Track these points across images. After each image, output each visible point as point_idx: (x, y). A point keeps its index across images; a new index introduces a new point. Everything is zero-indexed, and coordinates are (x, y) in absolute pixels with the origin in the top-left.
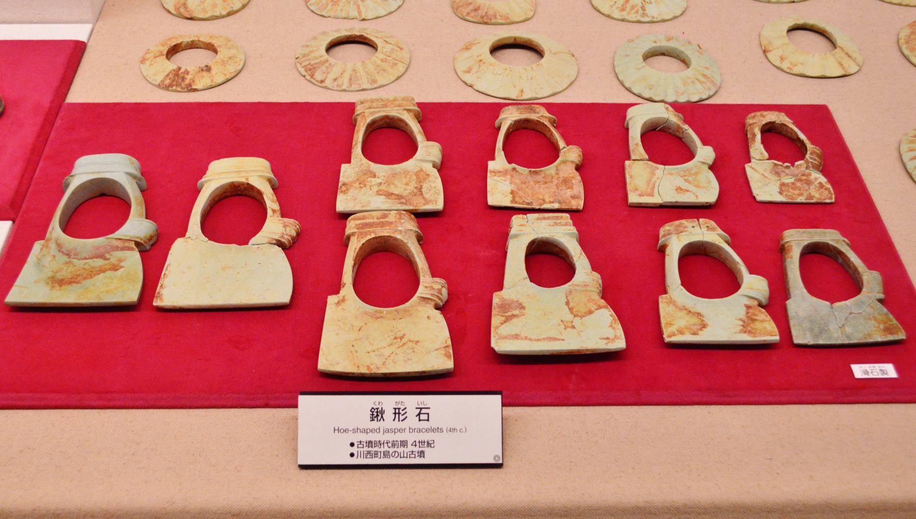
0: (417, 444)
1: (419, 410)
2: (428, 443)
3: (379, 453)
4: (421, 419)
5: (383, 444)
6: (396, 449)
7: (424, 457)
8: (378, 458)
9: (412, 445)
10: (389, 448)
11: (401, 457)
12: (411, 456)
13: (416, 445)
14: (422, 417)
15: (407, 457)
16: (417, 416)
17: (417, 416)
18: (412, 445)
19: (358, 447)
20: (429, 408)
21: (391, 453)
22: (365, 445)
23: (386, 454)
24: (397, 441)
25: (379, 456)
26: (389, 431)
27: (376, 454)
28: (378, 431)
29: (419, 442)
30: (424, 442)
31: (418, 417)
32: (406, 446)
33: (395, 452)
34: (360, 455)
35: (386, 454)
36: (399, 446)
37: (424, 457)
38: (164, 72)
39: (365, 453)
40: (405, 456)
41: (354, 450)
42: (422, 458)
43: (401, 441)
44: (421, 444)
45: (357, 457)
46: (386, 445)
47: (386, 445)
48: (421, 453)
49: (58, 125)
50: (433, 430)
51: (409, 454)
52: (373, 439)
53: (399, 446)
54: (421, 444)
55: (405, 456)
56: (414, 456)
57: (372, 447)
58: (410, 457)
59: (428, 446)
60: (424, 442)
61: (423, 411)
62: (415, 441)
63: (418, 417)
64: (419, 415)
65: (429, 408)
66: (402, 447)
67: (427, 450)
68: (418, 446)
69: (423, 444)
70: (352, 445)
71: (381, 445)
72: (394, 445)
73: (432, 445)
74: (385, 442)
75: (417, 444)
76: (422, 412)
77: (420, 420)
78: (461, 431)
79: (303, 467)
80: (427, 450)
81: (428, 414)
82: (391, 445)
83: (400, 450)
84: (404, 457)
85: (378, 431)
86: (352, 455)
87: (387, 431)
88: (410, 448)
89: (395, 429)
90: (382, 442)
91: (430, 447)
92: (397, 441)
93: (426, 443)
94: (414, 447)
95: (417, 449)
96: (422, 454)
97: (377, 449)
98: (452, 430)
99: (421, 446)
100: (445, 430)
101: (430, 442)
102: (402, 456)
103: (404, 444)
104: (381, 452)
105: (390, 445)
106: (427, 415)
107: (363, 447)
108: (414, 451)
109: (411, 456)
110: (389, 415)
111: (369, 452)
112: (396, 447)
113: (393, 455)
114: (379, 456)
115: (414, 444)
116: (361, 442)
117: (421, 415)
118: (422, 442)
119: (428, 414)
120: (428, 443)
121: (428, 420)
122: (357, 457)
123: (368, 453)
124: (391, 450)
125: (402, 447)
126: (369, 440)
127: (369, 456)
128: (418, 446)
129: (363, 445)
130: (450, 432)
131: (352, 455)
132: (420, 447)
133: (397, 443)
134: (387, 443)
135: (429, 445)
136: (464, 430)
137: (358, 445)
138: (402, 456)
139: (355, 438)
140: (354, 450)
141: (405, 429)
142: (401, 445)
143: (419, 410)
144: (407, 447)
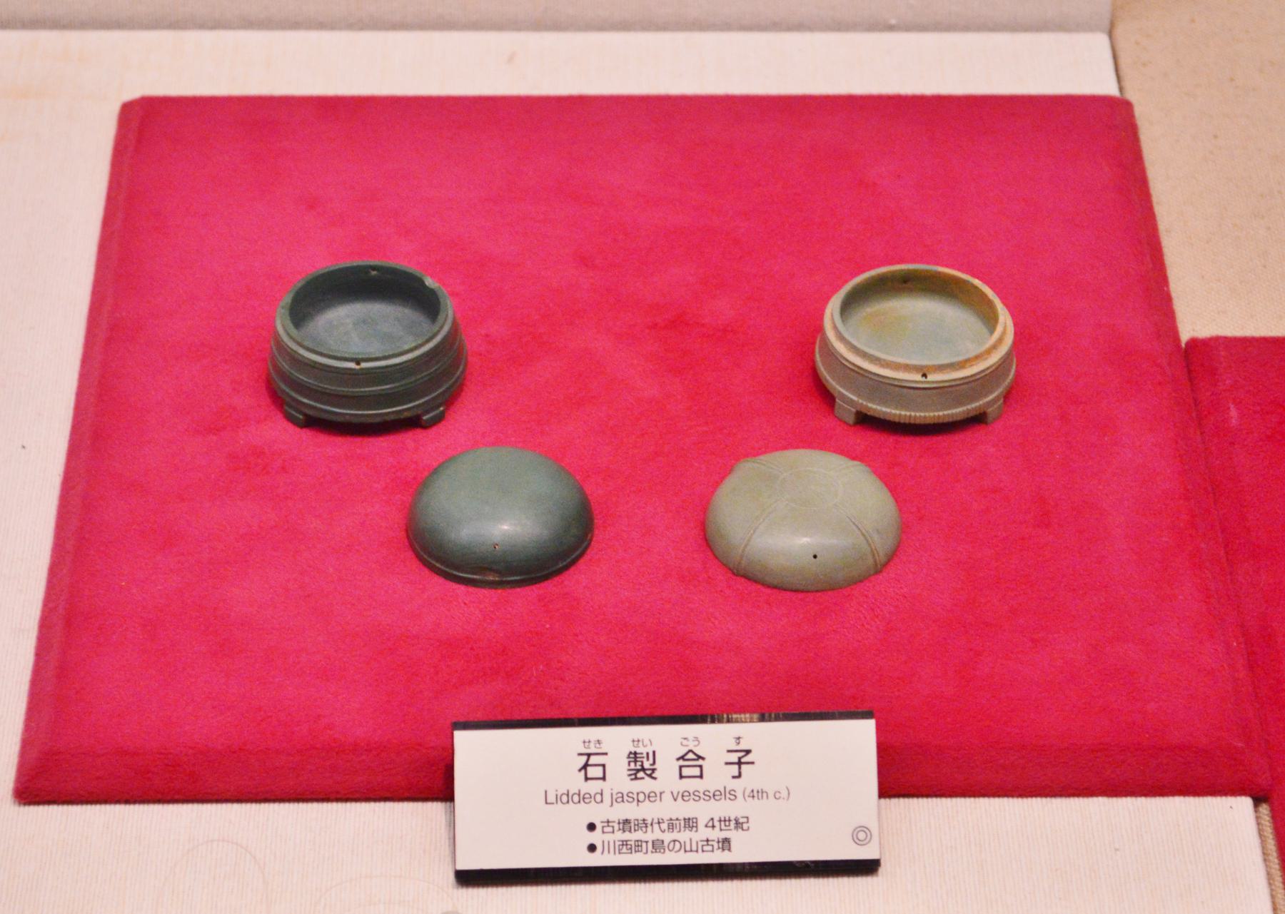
0: (717, 824)
1: (585, 758)
2: (737, 822)
3: (644, 845)
4: (589, 776)
5: (652, 824)
6: (675, 835)
7: (729, 850)
8: (641, 853)
9: (706, 826)
10: (663, 832)
11: (685, 851)
12: (705, 848)
13: (713, 827)
14: (592, 772)
15: (697, 851)
16: (580, 770)
17: (580, 770)
18: (706, 826)
19: (603, 832)
20: (606, 754)
21: (666, 844)
22: (616, 827)
23: (658, 846)
24: (677, 819)
25: (644, 850)
26: (625, 798)
27: (638, 845)
28: (598, 798)
29: (720, 821)
30: (730, 820)
31: (583, 772)
32: (694, 829)
33: (674, 841)
34: (607, 848)
35: (658, 846)
36: (682, 829)
37: (729, 850)
38: (924, 375)
39: (617, 844)
40: (694, 848)
41: (595, 837)
42: (726, 852)
43: (685, 819)
44: (723, 823)
45: (603, 853)
46: (656, 826)
47: (656, 826)
48: (723, 842)
49: (282, 304)
50: (583, 798)
51: (700, 844)
52: (631, 816)
53: (682, 829)
54: (723, 823)
55: (694, 848)
56: (710, 848)
57: (630, 831)
58: (703, 851)
59: (736, 828)
60: (730, 820)
61: (593, 760)
62: (712, 819)
63: (583, 772)
64: (585, 767)
65: (606, 754)
66: (687, 830)
67: (734, 835)
68: (717, 829)
69: (727, 823)
70: (592, 827)
71: (646, 827)
72: (671, 827)
73: (745, 826)
74: (656, 821)
75: (717, 824)
76: (590, 762)
77: (587, 779)
78: (778, 795)
79: (467, 878)
80: (734, 835)
81: (604, 766)
82: (666, 828)
83: (684, 836)
84: (691, 851)
85: (598, 798)
86: (592, 848)
87: (620, 800)
88: (704, 833)
89: (638, 794)
90: (649, 822)
91: (740, 830)
92: (677, 819)
93: (733, 823)
94: (711, 829)
95: (716, 834)
96: (726, 844)
97: (639, 835)
98: (755, 794)
99: (723, 827)
100: (740, 795)
101: (741, 820)
102: (688, 848)
103: (690, 823)
104: (647, 842)
105: (664, 826)
106: (601, 769)
107: (613, 832)
108: (710, 839)
109: (705, 848)
110: (667, 767)
111: (625, 843)
112: (675, 830)
113: (671, 848)
114: (644, 850)
115: (710, 824)
116: (608, 822)
117: (589, 769)
118: (725, 821)
119: (604, 766)
120: (737, 822)
121: (604, 778)
122: (603, 853)
123: (623, 845)
124: (667, 837)
125: (687, 830)
126: (625, 818)
127: (624, 850)
128: (717, 829)
129: (613, 827)
130: (751, 799)
131: (592, 848)
132: (721, 830)
133: (678, 822)
134: (659, 823)
135: (738, 825)
136: (785, 794)
137: (603, 827)
138: (688, 848)
139: (597, 813)
140: (595, 837)
141: (661, 793)
142: (685, 827)
143: (585, 758)
144: (697, 831)
